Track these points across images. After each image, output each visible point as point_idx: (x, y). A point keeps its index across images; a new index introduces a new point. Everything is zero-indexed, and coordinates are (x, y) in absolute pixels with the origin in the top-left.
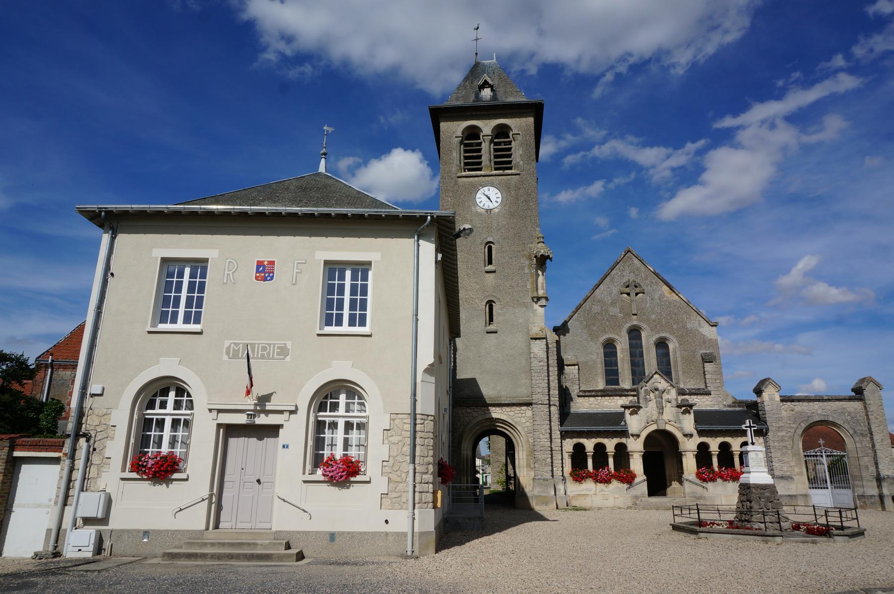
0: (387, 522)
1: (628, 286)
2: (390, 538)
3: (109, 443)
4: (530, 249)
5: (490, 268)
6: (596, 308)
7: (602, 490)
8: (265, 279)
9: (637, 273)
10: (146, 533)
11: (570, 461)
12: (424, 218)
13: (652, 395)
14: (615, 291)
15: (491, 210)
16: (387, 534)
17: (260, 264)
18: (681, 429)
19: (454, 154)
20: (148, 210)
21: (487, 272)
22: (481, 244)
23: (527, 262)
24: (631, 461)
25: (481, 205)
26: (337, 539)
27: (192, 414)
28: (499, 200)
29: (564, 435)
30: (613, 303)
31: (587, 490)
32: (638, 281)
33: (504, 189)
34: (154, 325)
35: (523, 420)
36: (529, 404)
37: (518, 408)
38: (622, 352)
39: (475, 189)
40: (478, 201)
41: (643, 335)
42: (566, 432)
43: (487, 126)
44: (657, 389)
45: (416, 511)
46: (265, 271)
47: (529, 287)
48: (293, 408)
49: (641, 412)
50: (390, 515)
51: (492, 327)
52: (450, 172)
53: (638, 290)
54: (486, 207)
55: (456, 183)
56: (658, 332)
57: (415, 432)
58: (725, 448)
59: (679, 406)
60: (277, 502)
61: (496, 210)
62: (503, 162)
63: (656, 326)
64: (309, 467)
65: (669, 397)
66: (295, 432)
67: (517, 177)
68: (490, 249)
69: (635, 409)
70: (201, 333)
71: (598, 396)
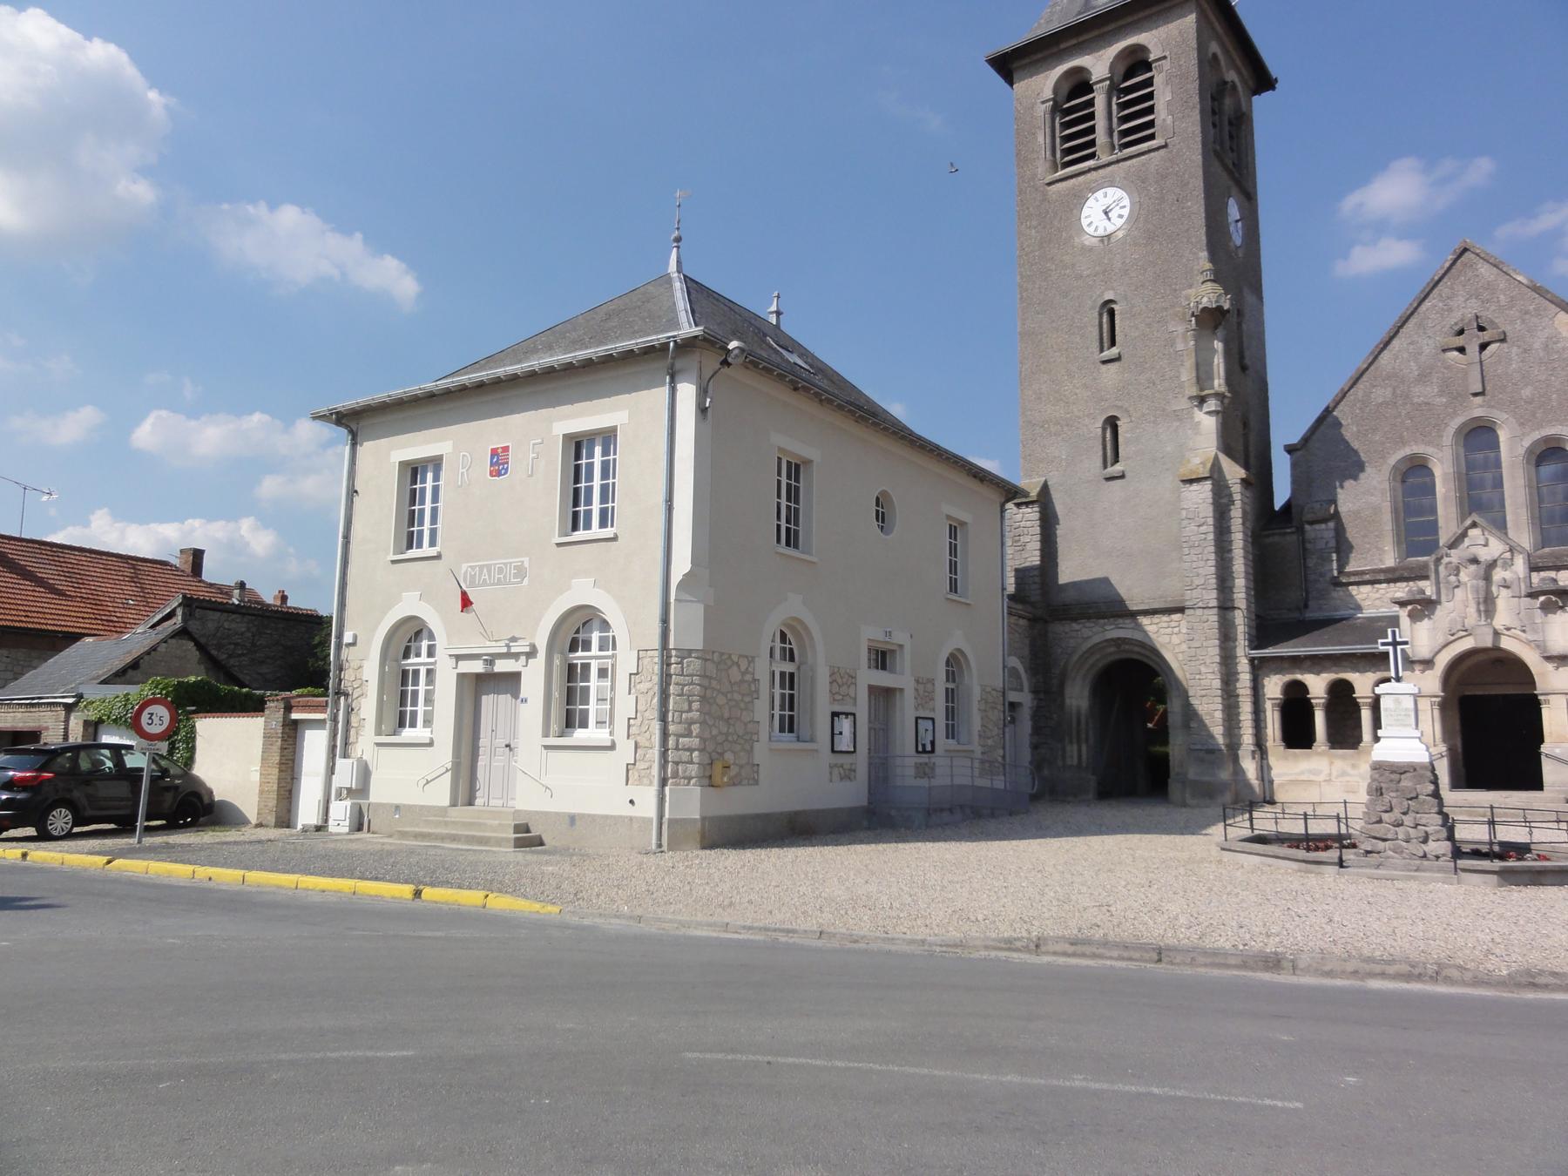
0: (632, 802)
1: (1461, 332)
2: (635, 826)
3: (363, 701)
4: (1187, 298)
5: (1108, 354)
6: (1381, 394)
7: (1344, 774)
8: (499, 474)
9: (1486, 295)
10: (397, 807)
11: (1277, 715)
12: (665, 346)
13: (1464, 576)
14: (1428, 346)
15: (1109, 236)
16: (631, 819)
17: (494, 452)
18: (1540, 646)
19: (1041, 139)
20: (635, 348)
21: (1104, 362)
22: (1092, 308)
23: (1181, 329)
24: (1546, 713)
25: (1090, 230)
26: (578, 823)
27: (613, 656)
28: (1126, 212)
29: (1259, 667)
30: (1423, 377)
31: (1310, 772)
32: (1487, 314)
33: (1135, 185)
34: (398, 551)
35: (1175, 640)
36: (1181, 610)
37: (1165, 618)
38: (1445, 481)
39: (1080, 199)
40: (1084, 222)
41: (1503, 436)
42: (1262, 659)
43: (1099, 64)
44: (1475, 561)
45: (667, 789)
46: (499, 461)
47: (1184, 378)
48: (527, 649)
49: (1440, 612)
50: (633, 791)
51: (1118, 468)
52: (1034, 176)
53: (1485, 336)
54: (1101, 232)
55: (1044, 194)
56: (1540, 426)
57: (669, 676)
58: (1341, 695)
59: (1533, 595)
60: (519, 774)
61: (1120, 234)
62: (1136, 124)
63: (1534, 414)
64: (554, 727)
65: (1507, 575)
66: (534, 678)
67: (1162, 152)
68: (1112, 313)
69: (1423, 607)
70: (615, 539)
71: (1379, 582)
